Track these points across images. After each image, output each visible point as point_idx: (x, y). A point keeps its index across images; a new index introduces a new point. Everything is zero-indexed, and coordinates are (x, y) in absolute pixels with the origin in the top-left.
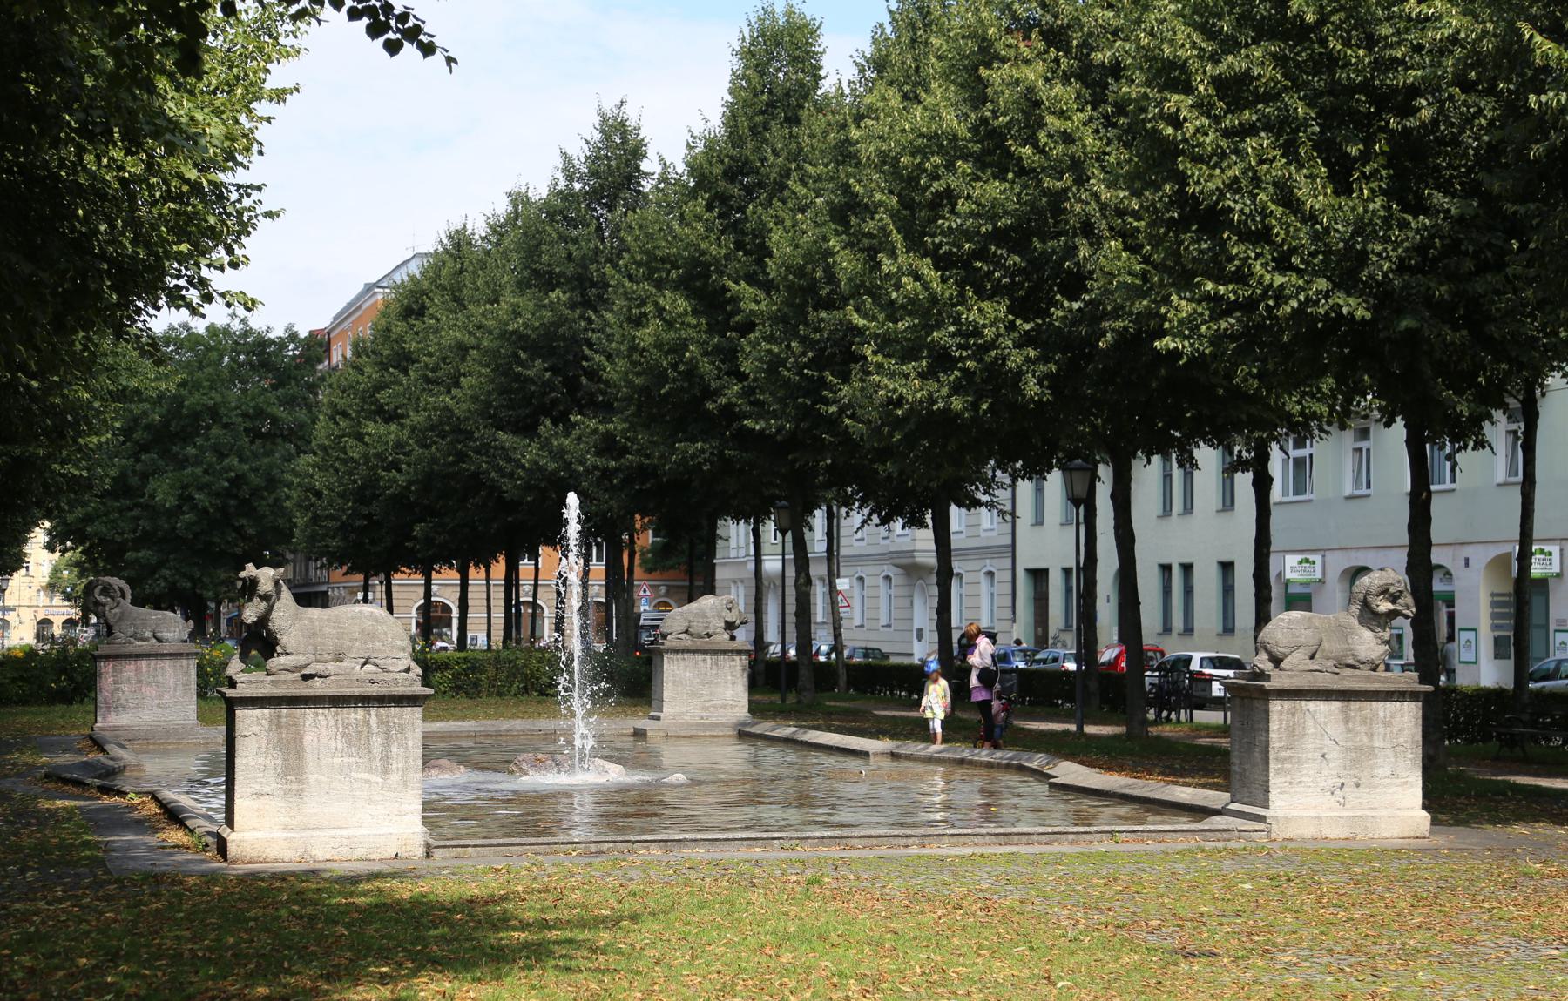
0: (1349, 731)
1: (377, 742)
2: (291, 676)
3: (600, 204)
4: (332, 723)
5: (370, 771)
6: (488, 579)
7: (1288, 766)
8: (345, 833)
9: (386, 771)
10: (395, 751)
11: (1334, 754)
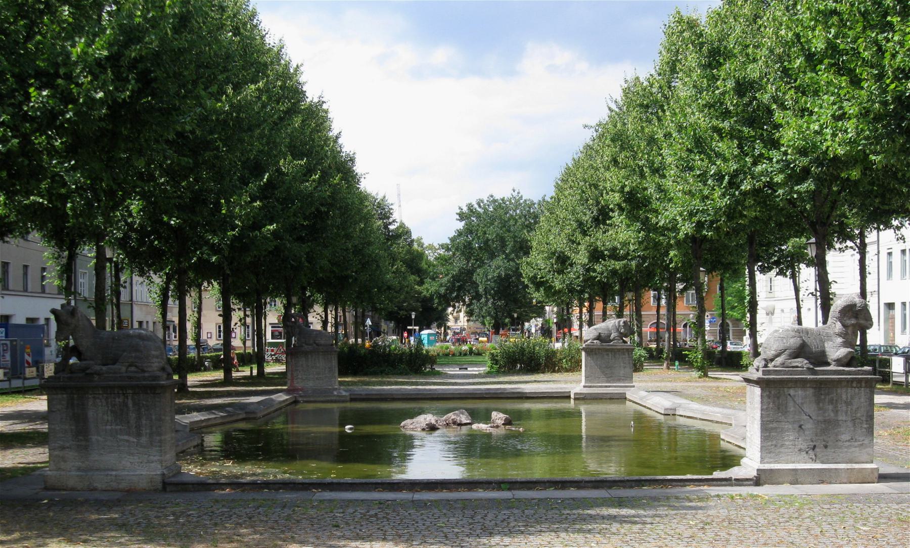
0: (820, 409)
1: (133, 416)
2: (81, 375)
4: (104, 404)
5: (129, 434)
6: (797, 290)
8: (114, 473)
9: (139, 435)
10: (144, 422)
11: (809, 426)
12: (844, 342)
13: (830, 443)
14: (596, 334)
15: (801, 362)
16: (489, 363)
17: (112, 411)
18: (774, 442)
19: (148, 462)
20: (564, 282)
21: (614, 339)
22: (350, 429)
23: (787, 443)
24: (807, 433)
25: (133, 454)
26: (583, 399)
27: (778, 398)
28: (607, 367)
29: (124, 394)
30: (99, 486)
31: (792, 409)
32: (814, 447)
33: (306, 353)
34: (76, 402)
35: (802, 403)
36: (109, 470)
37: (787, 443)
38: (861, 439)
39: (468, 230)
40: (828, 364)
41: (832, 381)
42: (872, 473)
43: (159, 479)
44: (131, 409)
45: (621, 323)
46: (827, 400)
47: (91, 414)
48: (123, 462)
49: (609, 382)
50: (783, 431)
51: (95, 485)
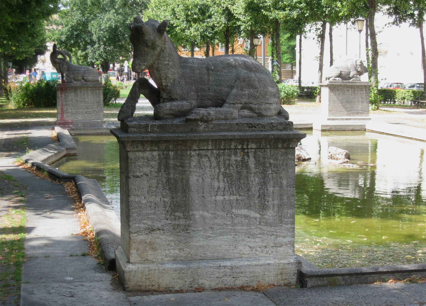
4: (214, 164)
5: (249, 207)
8: (228, 263)
9: (263, 207)
10: (271, 189)
14: (337, 72)
17: (225, 175)
19: (276, 246)
20: (198, 30)
21: (353, 77)
25: (253, 236)
26: (329, 130)
28: (348, 102)
29: (243, 149)
30: (206, 283)
33: (75, 89)
34: (171, 162)
36: (224, 259)
43: (293, 269)
44: (253, 170)
47: (194, 179)
48: (240, 248)
49: (349, 115)
51: (201, 281)
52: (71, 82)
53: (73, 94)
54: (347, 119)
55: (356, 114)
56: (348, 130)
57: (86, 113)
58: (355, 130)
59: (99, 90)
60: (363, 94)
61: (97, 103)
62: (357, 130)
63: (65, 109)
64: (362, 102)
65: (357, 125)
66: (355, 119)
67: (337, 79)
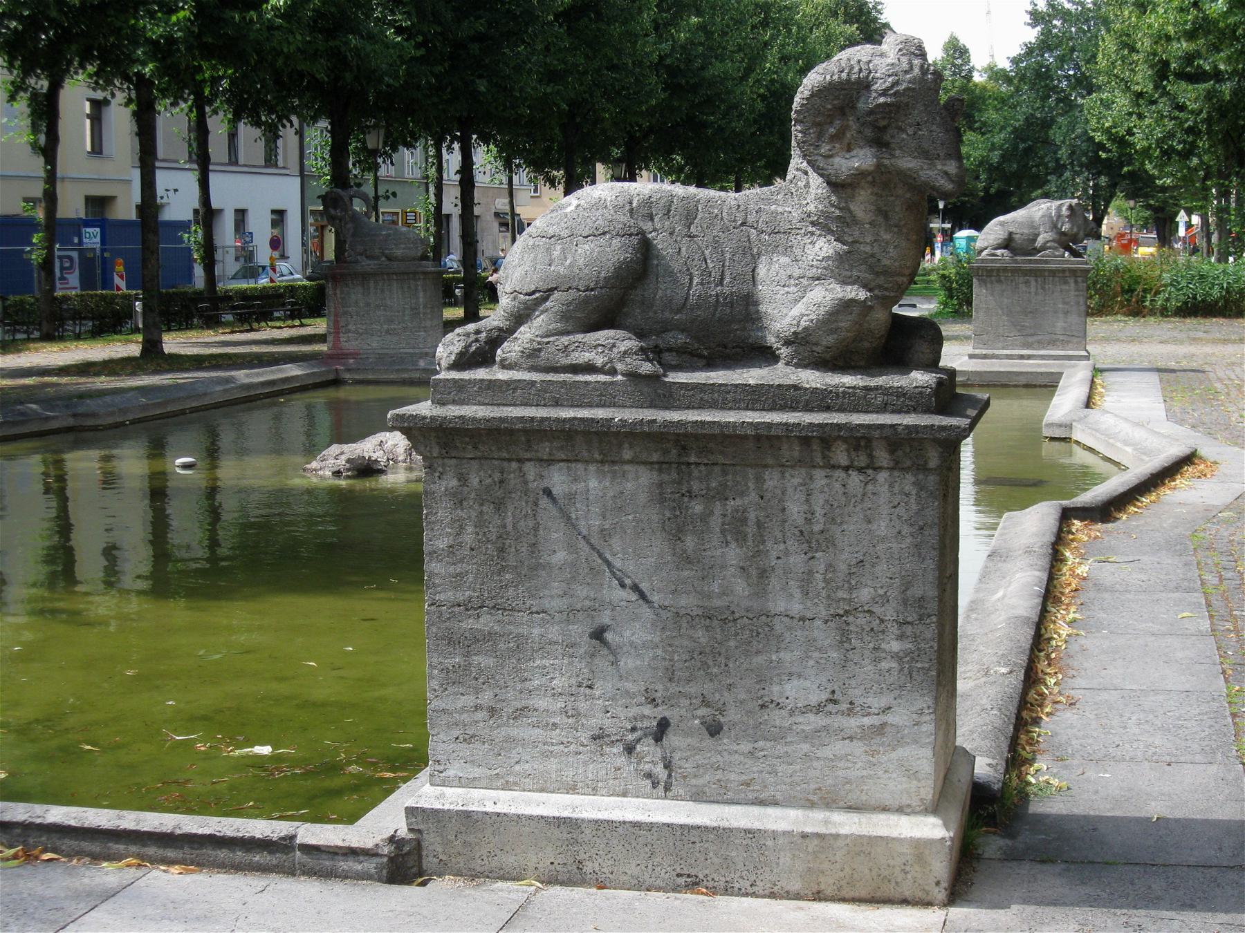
3: (137, 61)
7: (482, 660)
11: (636, 632)
12: (840, 258)
13: (733, 715)
15: (612, 347)
16: (942, 295)
18: (486, 697)
21: (1043, 248)
22: (186, 466)
23: (542, 703)
24: (628, 662)
27: (499, 505)
31: (561, 556)
32: (661, 729)
33: (365, 277)
35: (604, 534)
37: (542, 703)
38: (876, 703)
39: (1045, 44)
40: (766, 355)
41: (726, 438)
42: (920, 859)
45: (1065, 211)
46: (716, 522)
50: (521, 649)
52: (357, 262)
53: (359, 289)
54: (1022, 357)
55: (1049, 343)
56: (1016, 386)
57: (387, 332)
58: (1035, 386)
59: (415, 280)
60: (1068, 291)
61: (412, 309)
62: (1040, 386)
63: (342, 324)
64: (1066, 313)
65: (1041, 373)
66: (1042, 357)
67: (999, 252)
